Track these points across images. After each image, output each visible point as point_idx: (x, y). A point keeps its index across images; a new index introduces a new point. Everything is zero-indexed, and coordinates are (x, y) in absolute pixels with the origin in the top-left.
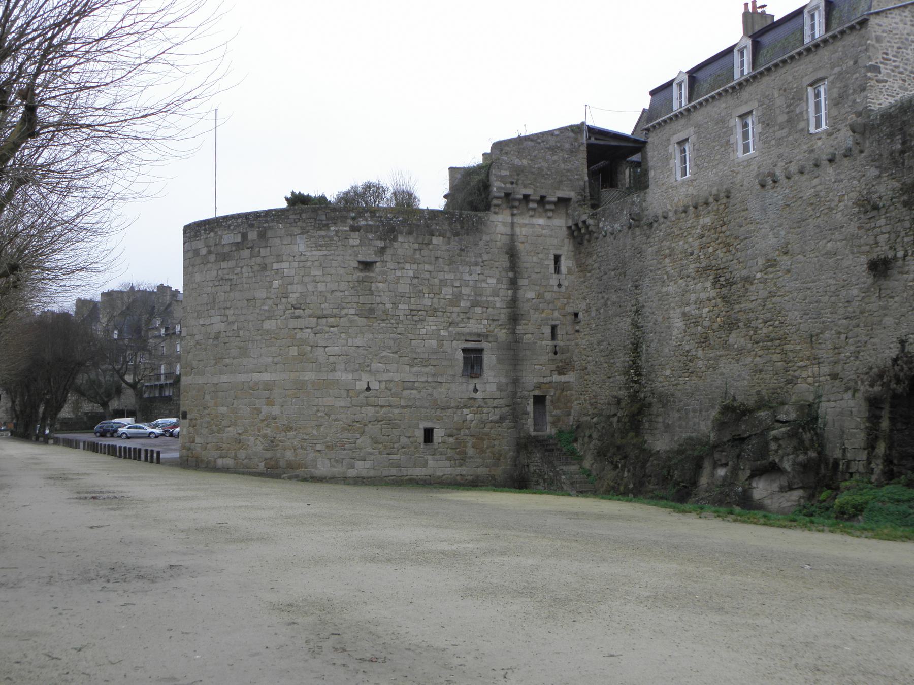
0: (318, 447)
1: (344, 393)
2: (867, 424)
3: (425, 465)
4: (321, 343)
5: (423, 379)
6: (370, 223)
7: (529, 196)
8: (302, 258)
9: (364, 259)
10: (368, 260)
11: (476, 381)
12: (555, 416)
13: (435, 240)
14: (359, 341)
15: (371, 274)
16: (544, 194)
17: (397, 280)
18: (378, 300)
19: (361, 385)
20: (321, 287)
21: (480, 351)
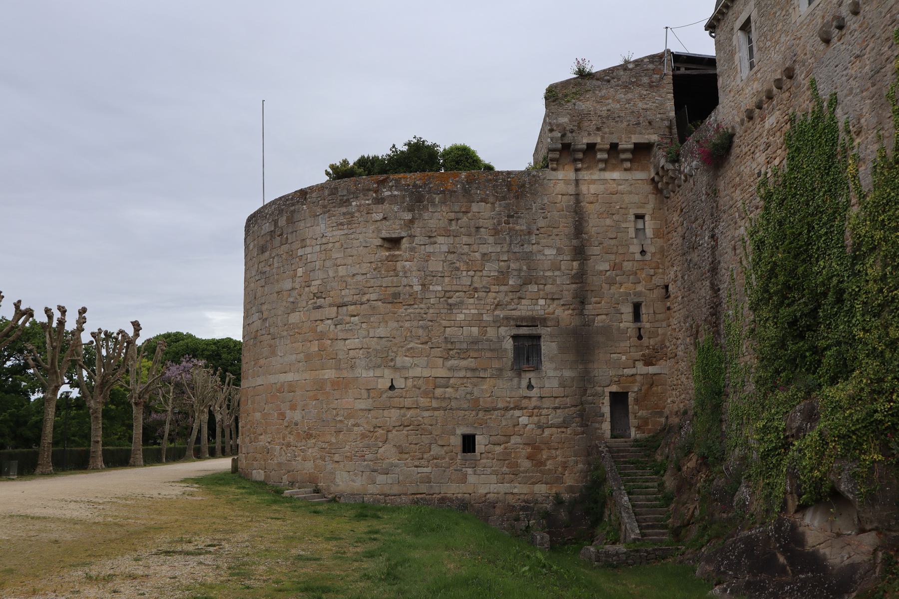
0: (337, 457)
1: (365, 394)
2: (568, 373)
3: (464, 479)
4: (341, 335)
5: (462, 374)
6: (396, 193)
7: (594, 145)
8: (324, 240)
9: (388, 236)
10: (393, 236)
11: (531, 375)
12: (640, 418)
13: (475, 207)
14: (381, 331)
15: (397, 253)
16: (615, 141)
17: (427, 258)
18: (405, 281)
19: (385, 384)
20: (342, 271)
21: (538, 337)
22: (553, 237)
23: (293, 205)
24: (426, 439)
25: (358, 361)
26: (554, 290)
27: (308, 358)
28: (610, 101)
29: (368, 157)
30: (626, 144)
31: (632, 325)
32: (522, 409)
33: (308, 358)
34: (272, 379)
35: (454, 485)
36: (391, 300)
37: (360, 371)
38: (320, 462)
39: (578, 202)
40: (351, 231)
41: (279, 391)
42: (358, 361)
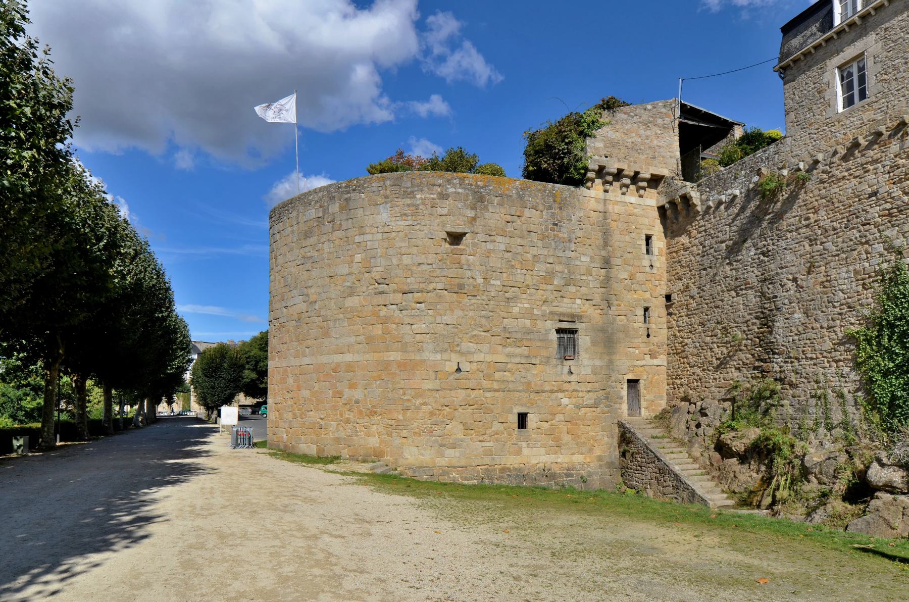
0: (405, 433)
2: (598, 363)
3: (519, 452)
4: (407, 320)
5: (517, 360)
6: (460, 190)
8: (386, 229)
9: (453, 230)
13: (527, 213)
16: (638, 170)
17: (488, 254)
18: (469, 274)
20: (406, 260)
21: (574, 331)
22: (587, 246)
23: (348, 192)
24: (489, 417)
25: (425, 345)
26: (587, 292)
27: (370, 340)
28: (634, 135)
30: (645, 174)
31: (643, 325)
32: (564, 391)
33: (370, 340)
34: (324, 359)
35: (512, 457)
36: (456, 289)
37: (427, 354)
39: (605, 218)
40: (416, 222)
41: (334, 371)
42: (425, 345)
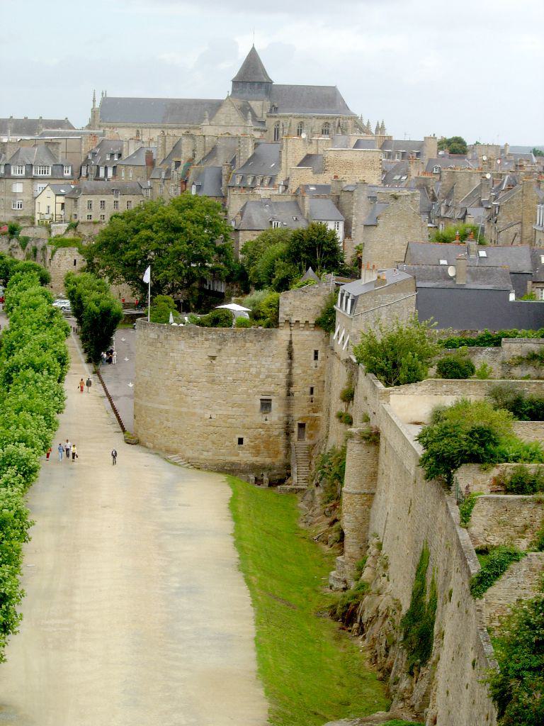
13: (248, 345)
19: (207, 416)
20: (191, 367)
21: (270, 400)
29: (229, 504)
38: (179, 445)
